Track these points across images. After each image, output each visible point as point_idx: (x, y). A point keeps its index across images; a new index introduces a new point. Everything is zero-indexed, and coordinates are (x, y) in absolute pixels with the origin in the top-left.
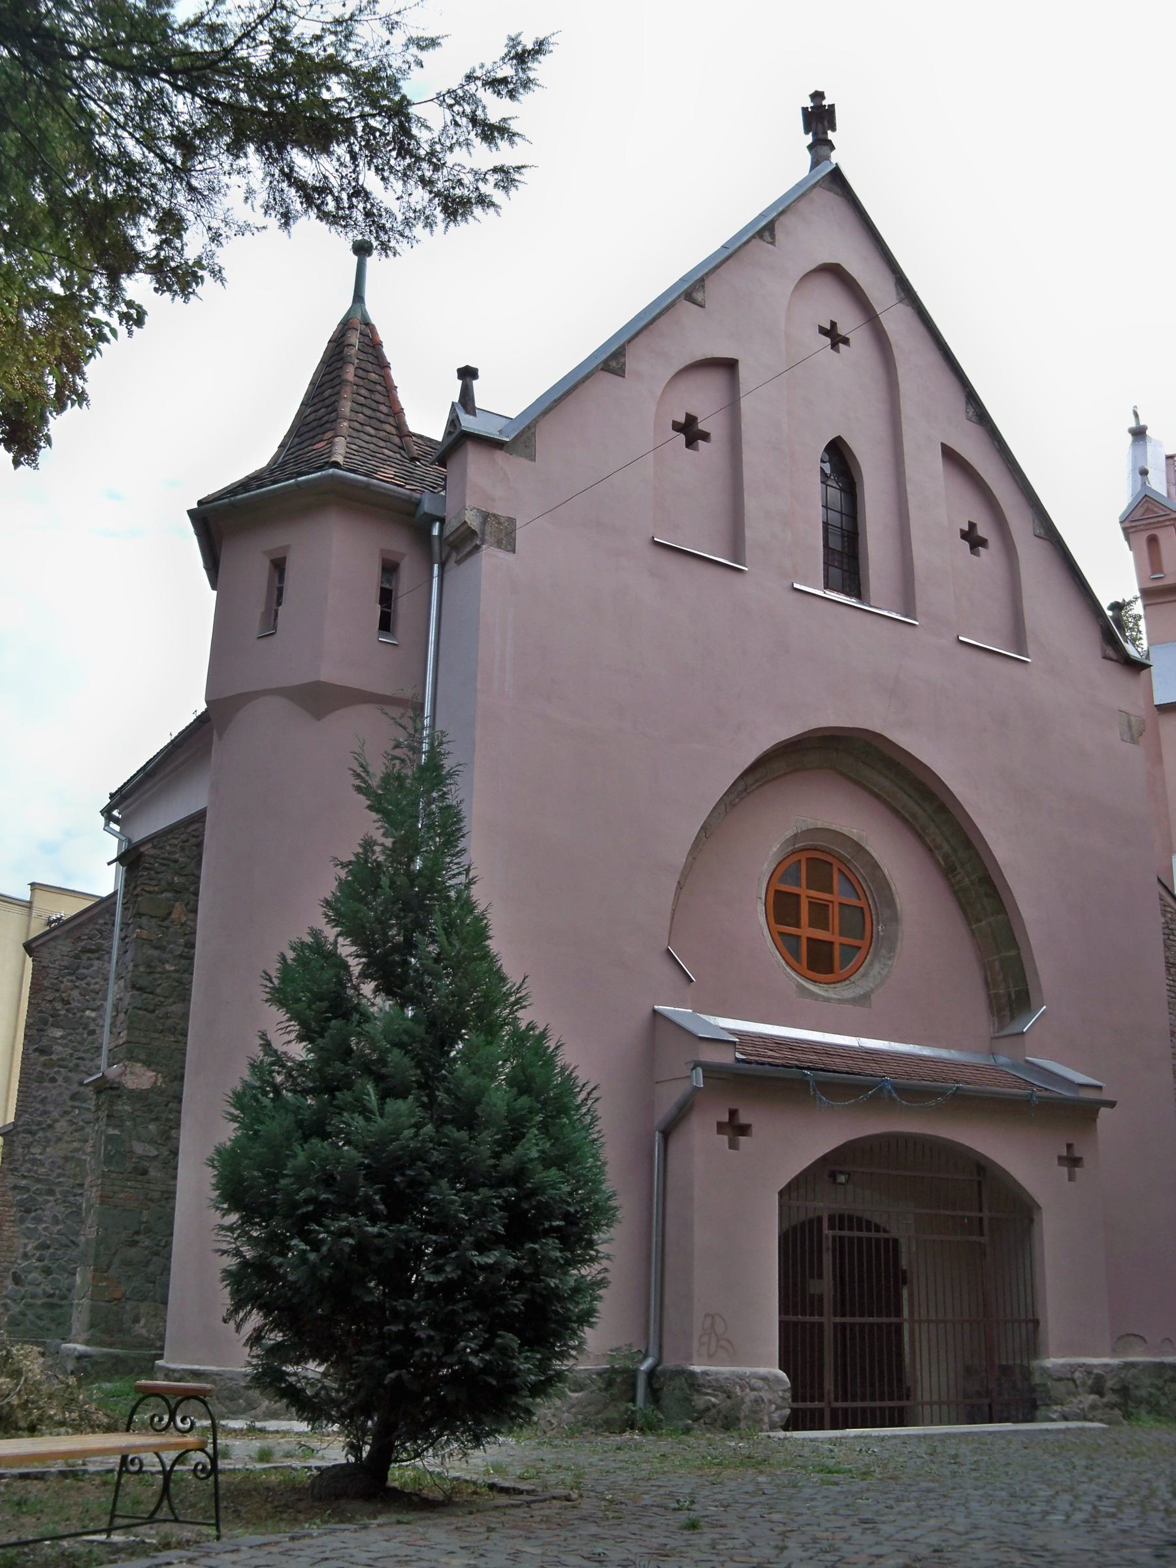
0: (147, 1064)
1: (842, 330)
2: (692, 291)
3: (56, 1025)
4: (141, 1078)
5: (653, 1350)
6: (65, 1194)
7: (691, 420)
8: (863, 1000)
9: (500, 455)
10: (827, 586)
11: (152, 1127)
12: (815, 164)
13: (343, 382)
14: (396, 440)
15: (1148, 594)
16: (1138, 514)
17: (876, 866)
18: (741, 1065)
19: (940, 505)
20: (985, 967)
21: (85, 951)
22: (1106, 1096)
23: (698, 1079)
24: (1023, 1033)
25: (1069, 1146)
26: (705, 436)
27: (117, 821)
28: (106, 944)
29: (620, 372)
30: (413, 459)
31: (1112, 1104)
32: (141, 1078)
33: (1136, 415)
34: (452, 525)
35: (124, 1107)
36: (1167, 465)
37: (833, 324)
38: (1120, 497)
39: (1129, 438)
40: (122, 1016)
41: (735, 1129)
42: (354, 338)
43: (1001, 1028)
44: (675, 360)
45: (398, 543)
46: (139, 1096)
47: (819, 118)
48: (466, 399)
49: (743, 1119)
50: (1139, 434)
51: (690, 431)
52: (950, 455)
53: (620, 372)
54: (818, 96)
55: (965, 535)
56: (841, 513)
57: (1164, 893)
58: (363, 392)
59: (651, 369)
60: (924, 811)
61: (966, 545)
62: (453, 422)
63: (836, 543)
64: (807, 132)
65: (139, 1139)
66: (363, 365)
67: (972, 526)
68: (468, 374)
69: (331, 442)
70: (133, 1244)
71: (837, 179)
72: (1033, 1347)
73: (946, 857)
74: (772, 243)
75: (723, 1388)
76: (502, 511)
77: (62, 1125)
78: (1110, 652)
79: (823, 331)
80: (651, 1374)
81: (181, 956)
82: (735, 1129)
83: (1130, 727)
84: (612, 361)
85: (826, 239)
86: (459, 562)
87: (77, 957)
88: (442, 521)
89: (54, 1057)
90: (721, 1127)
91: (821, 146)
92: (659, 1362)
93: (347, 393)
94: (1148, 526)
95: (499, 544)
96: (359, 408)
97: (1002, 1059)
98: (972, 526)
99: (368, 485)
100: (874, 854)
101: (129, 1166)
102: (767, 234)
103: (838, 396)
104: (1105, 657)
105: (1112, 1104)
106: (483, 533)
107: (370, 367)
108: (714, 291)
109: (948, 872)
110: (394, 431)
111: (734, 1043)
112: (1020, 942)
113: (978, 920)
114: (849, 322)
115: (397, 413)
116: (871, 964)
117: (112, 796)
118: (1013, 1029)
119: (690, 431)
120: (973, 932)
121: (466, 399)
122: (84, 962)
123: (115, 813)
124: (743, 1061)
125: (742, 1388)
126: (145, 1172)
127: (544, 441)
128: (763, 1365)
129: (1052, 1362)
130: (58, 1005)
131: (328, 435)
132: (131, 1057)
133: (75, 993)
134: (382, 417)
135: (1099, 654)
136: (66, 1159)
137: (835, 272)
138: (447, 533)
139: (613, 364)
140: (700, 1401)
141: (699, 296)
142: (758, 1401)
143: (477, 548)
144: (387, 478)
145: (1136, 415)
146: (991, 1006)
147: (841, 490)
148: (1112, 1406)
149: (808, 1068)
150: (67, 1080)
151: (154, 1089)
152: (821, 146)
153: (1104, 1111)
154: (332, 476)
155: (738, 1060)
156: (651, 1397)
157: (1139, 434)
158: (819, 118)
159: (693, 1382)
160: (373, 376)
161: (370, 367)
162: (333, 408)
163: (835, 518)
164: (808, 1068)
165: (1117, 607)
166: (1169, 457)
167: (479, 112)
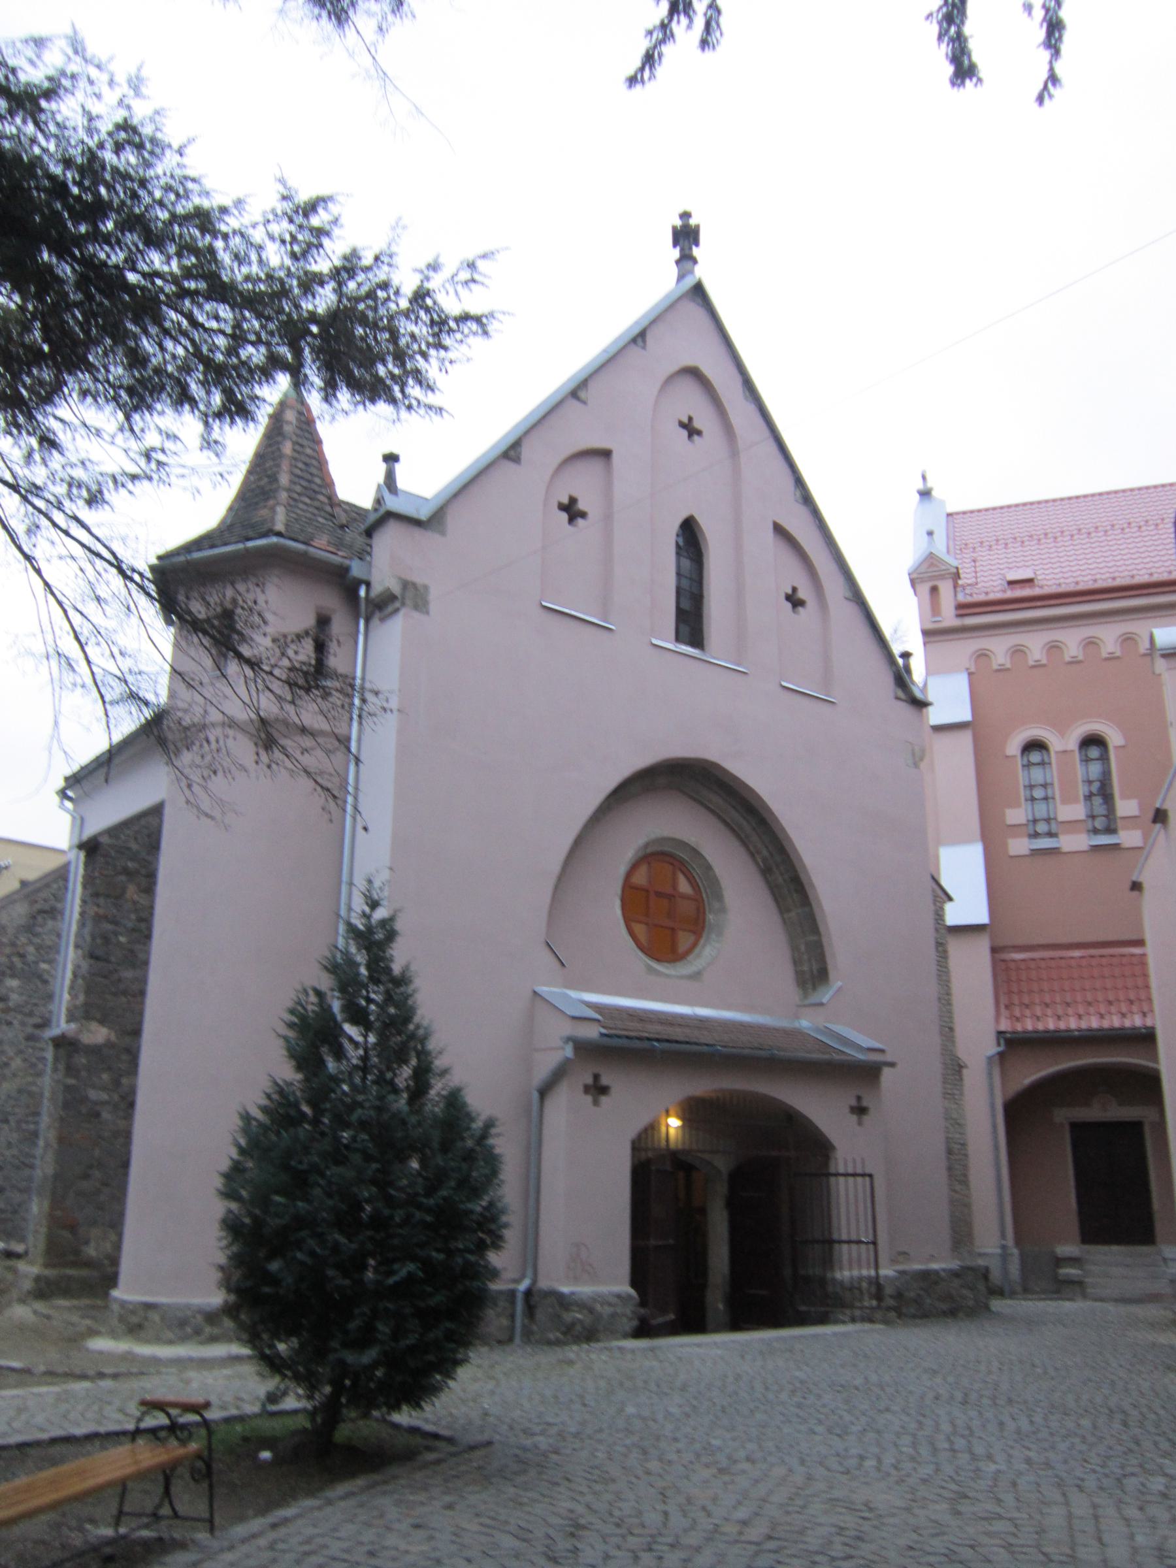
0: (102, 1022)
1: (697, 424)
2: (577, 392)
3: (13, 976)
4: (98, 1034)
5: (529, 1272)
6: (19, 1122)
7: (573, 500)
8: (696, 976)
9: (417, 532)
10: (678, 639)
11: (105, 1076)
12: (681, 277)
13: (281, 456)
14: (328, 509)
15: (929, 634)
16: (923, 569)
17: (709, 867)
18: (606, 1039)
19: (774, 571)
20: (794, 948)
21: (41, 912)
22: (888, 1058)
23: (569, 1052)
24: (822, 1004)
25: (859, 1098)
26: (583, 515)
27: (70, 799)
28: (59, 905)
29: (517, 460)
30: (342, 527)
31: (892, 1065)
32: (98, 1034)
33: (924, 478)
34: (377, 589)
35: (81, 1060)
36: (947, 522)
37: (690, 419)
38: (908, 556)
39: (918, 496)
40: (80, 981)
41: (598, 1090)
42: (290, 416)
43: (805, 995)
44: (560, 456)
45: (330, 600)
46: (95, 1051)
47: (686, 236)
48: (390, 481)
49: (604, 1081)
50: (925, 494)
51: (572, 511)
52: (779, 530)
53: (517, 460)
54: (685, 216)
55: (789, 598)
56: (690, 579)
57: (935, 887)
58: (300, 465)
59: (540, 459)
60: (748, 821)
61: (789, 605)
62: (379, 501)
63: (686, 605)
64: (675, 246)
65: (94, 1087)
66: (300, 441)
67: (794, 589)
68: (391, 459)
69: (273, 509)
70: (86, 1176)
71: (698, 291)
72: (828, 1261)
73: (764, 860)
74: (644, 348)
75: (585, 1306)
76: (419, 579)
77: (17, 1063)
78: (901, 694)
79: (682, 425)
80: (528, 1293)
81: (133, 930)
82: (598, 1090)
83: (913, 754)
84: (511, 452)
85: (687, 346)
86: (382, 620)
87: (34, 917)
88: (368, 584)
89: (11, 1004)
90: (587, 1089)
91: (686, 259)
92: (534, 1281)
93: (285, 466)
94: (931, 578)
95: (416, 607)
96: (296, 480)
97: (804, 1024)
98: (794, 589)
99: (305, 554)
100: (708, 858)
101: (84, 1110)
102: (639, 341)
103: (693, 482)
104: (897, 698)
105: (892, 1065)
106: (403, 598)
107: (305, 442)
108: (592, 393)
109: (766, 872)
110: (326, 501)
111: (598, 1021)
112: (822, 929)
113: (789, 911)
114: (705, 420)
115: (328, 484)
116: (703, 947)
117: (67, 779)
118: (814, 998)
119: (572, 511)
120: (784, 921)
121: (390, 481)
122: (40, 919)
123: (70, 793)
124: (606, 1035)
125: (602, 1305)
126: (97, 1115)
127: (453, 521)
128: (609, 1280)
129: (844, 1274)
130: (16, 959)
131: (271, 502)
132: (88, 1016)
133: (31, 949)
134: (317, 488)
135: (891, 695)
136: (20, 1091)
137: (693, 372)
138: (373, 594)
139: (512, 453)
140: (568, 1317)
141: (582, 394)
142: (614, 1315)
143: (397, 610)
144: (321, 547)
145: (924, 478)
146: (797, 982)
147: (691, 559)
148: (889, 1309)
149: (658, 1040)
150: (23, 1024)
151: (109, 1044)
152: (686, 259)
153: (886, 1071)
154: (276, 547)
155: (602, 1035)
156: (555, 1322)
157: (925, 494)
158: (686, 236)
159: (563, 1302)
160: (309, 451)
161: (305, 442)
162: (274, 479)
163: (685, 583)
164: (658, 1040)
165: (906, 655)
166: (949, 515)
167: (435, 317)
